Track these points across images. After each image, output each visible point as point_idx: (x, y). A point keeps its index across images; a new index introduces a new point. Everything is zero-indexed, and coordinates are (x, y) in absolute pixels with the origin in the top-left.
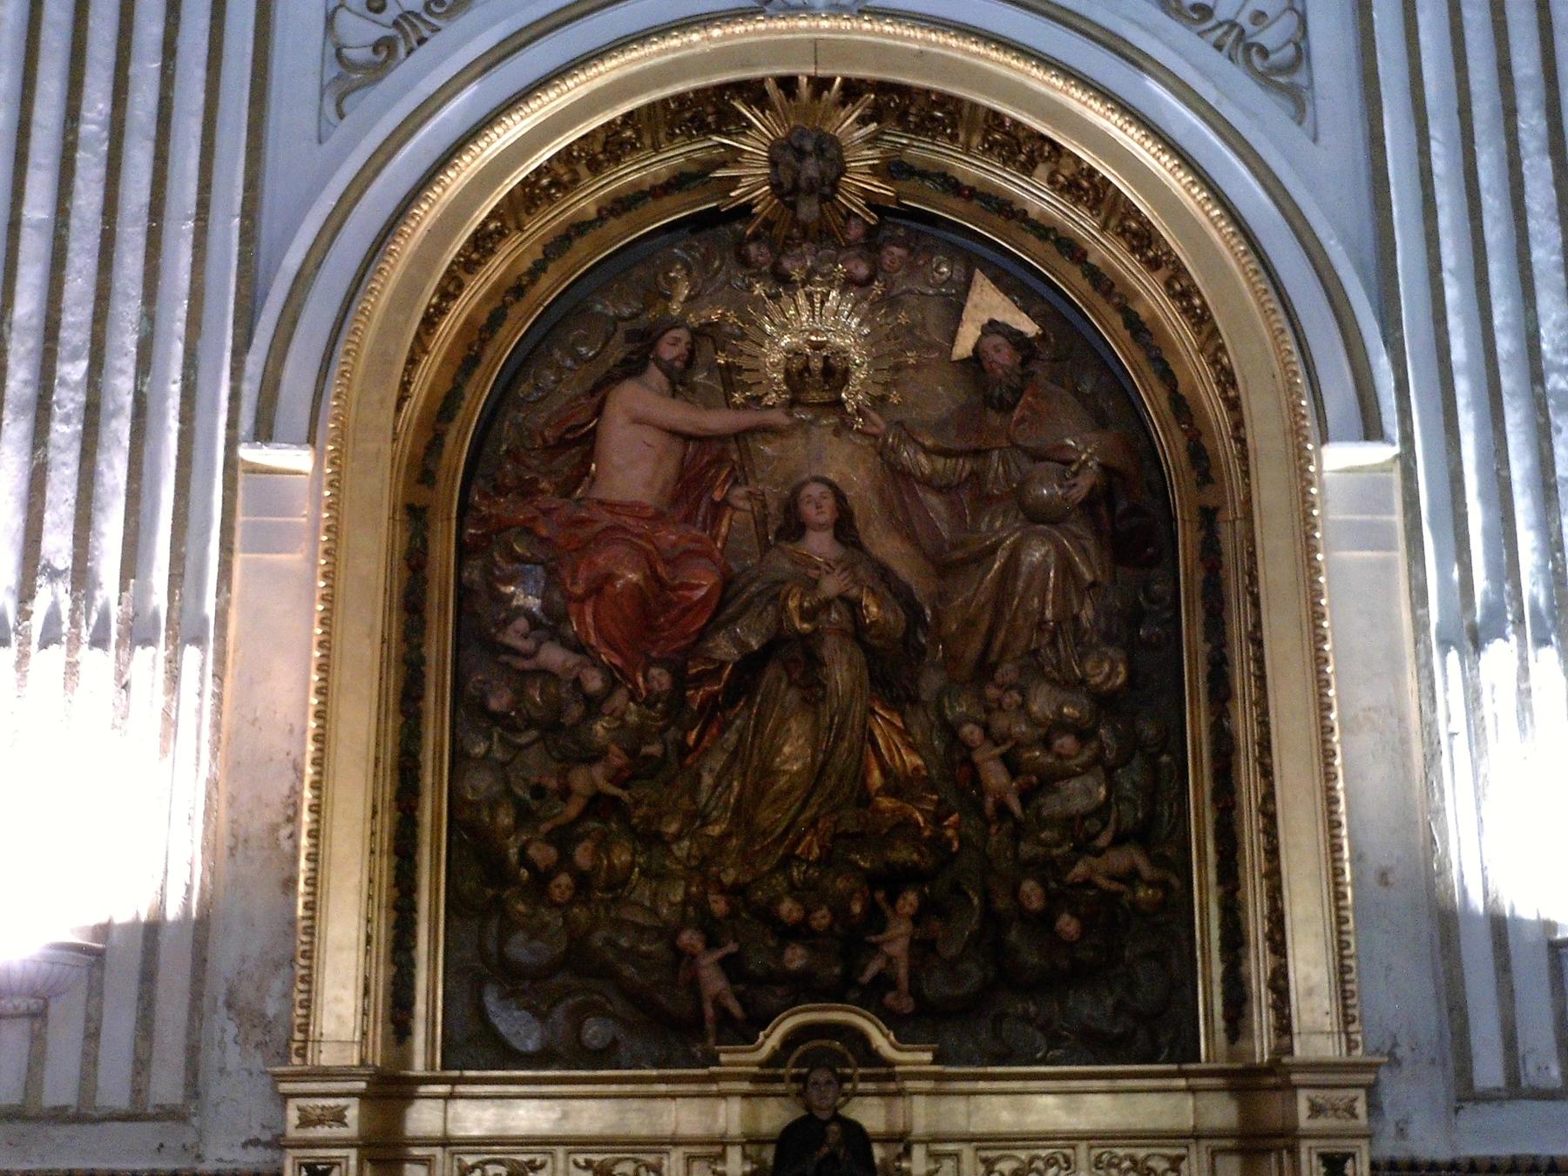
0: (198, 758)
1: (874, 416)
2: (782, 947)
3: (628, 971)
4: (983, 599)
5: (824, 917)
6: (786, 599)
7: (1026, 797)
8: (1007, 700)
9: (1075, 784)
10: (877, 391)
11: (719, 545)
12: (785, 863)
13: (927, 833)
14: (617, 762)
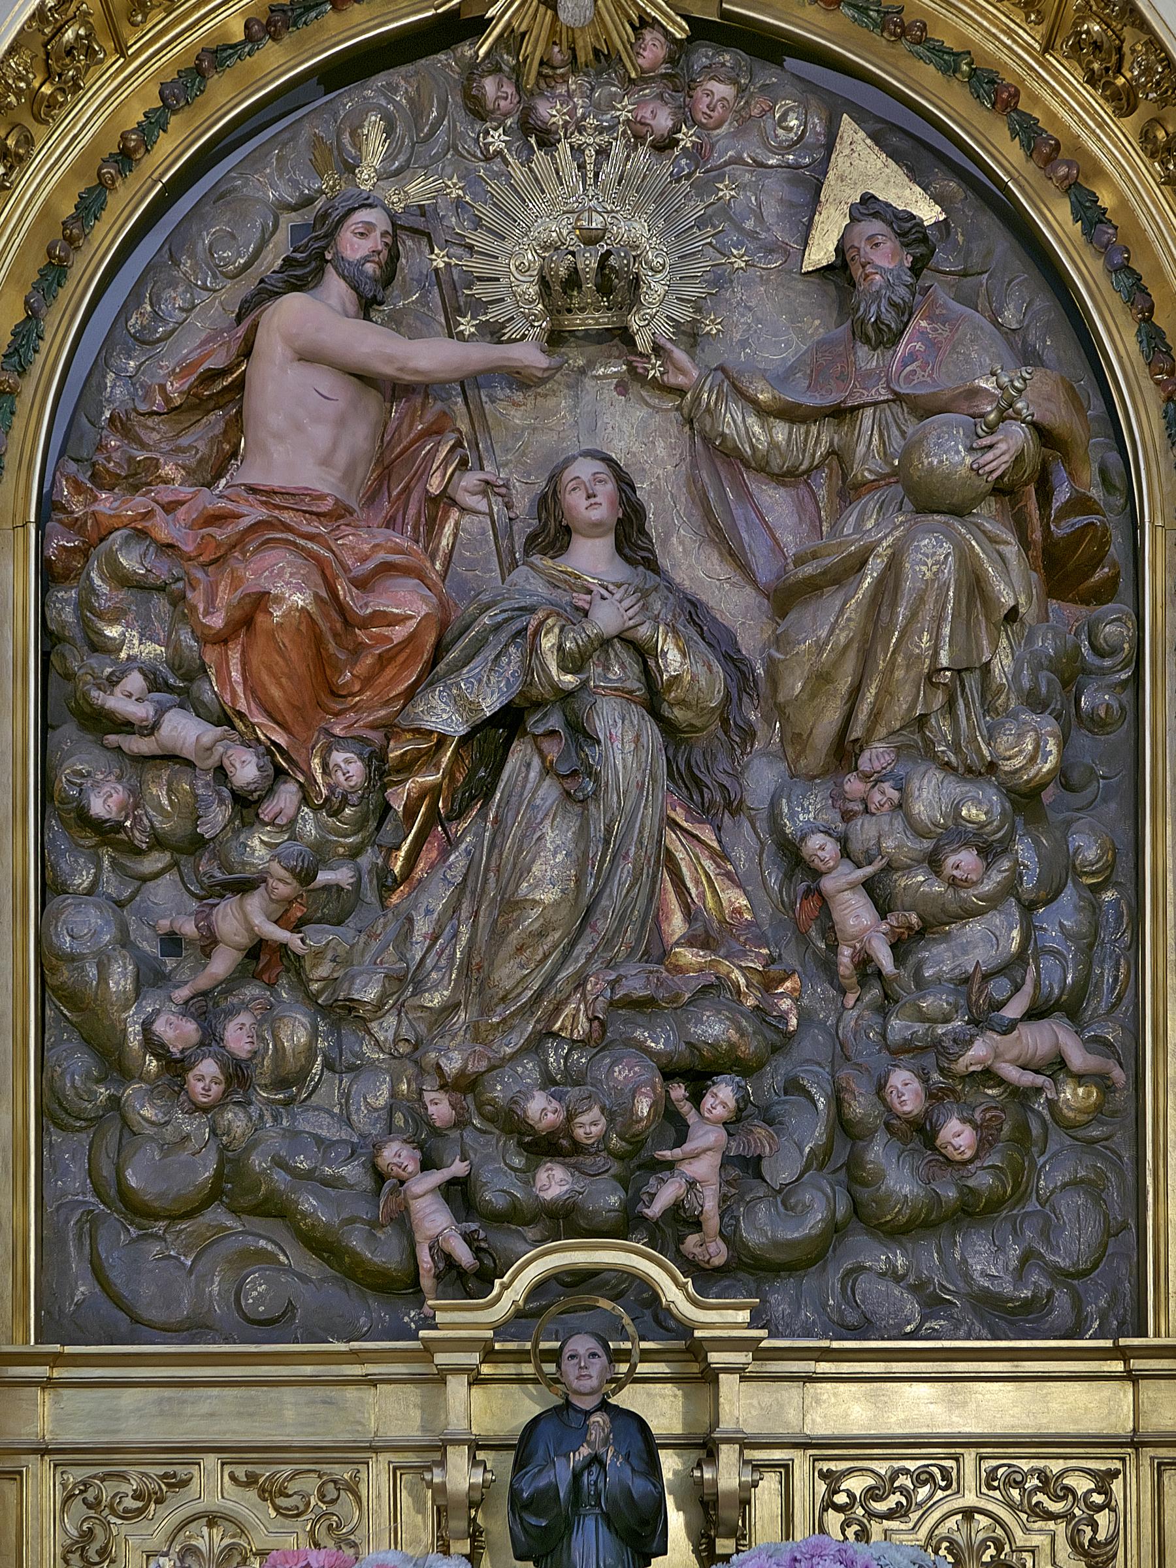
1: (679, 355)
2: (530, 1170)
3: (308, 1203)
4: (843, 639)
5: (594, 1123)
6: (537, 632)
7: (900, 947)
8: (877, 797)
9: (975, 928)
10: (684, 314)
11: (438, 567)
12: (535, 1045)
13: (750, 1002)
14: (283, 890)
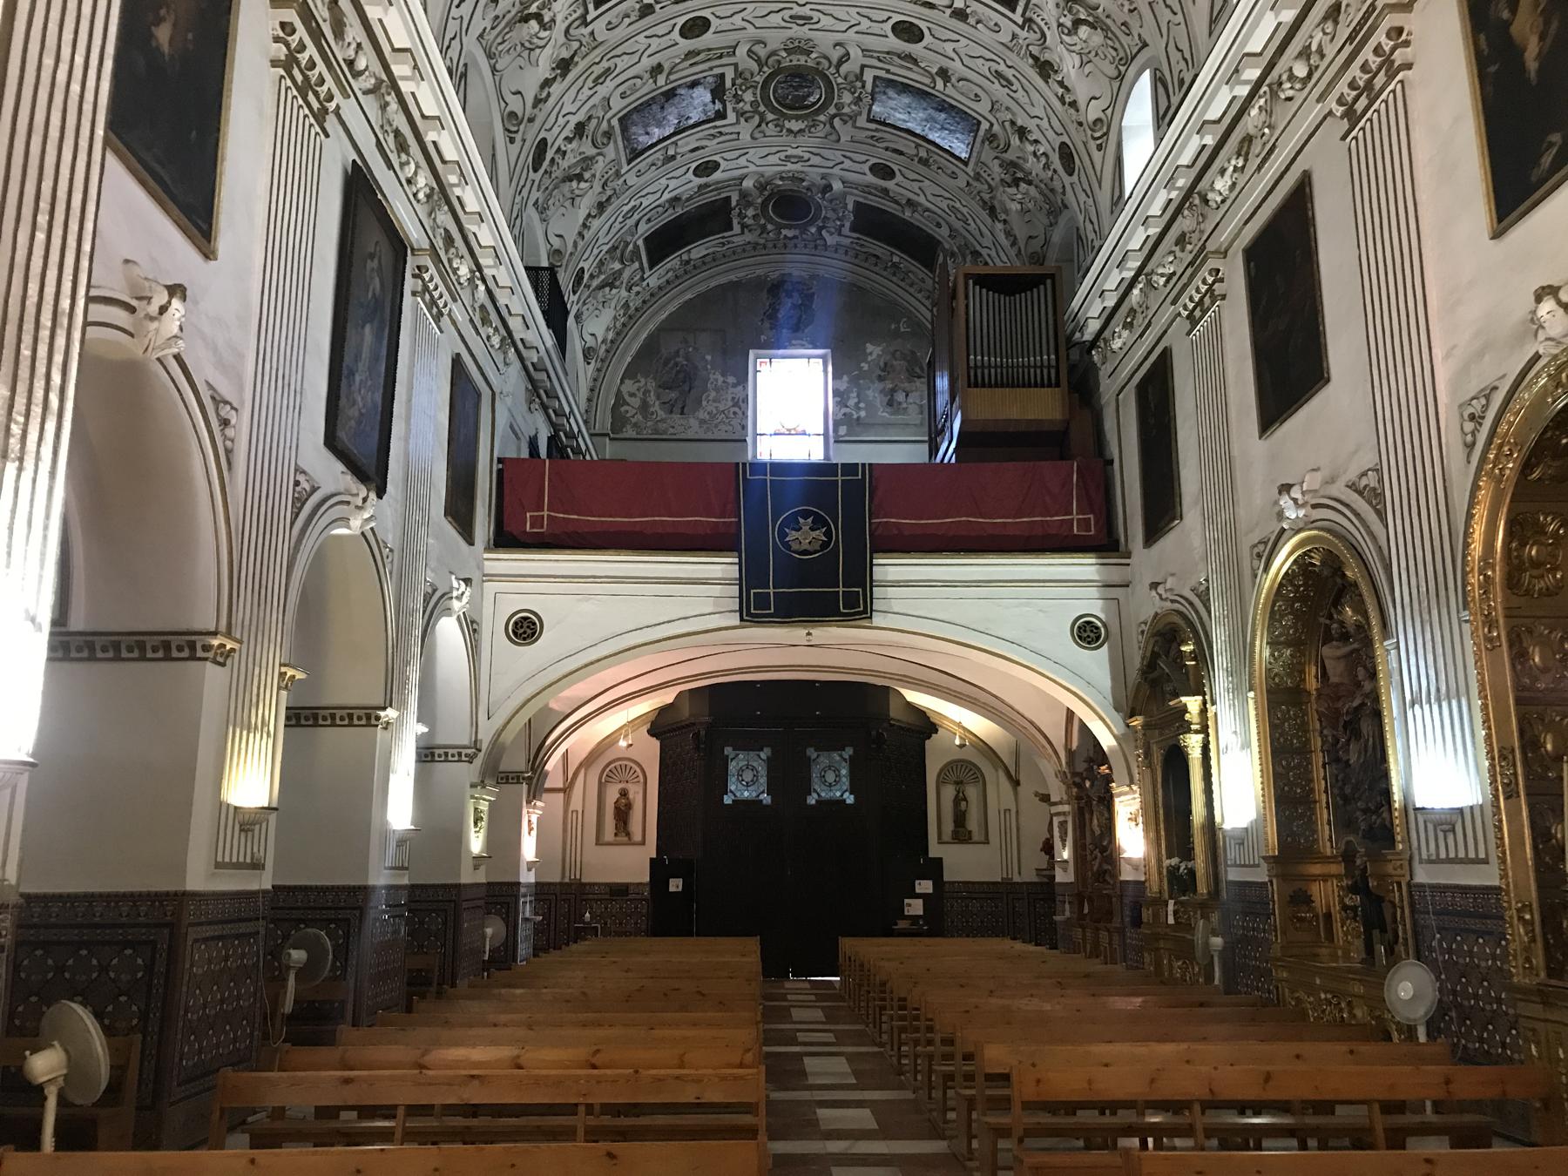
0: (9, 546)
